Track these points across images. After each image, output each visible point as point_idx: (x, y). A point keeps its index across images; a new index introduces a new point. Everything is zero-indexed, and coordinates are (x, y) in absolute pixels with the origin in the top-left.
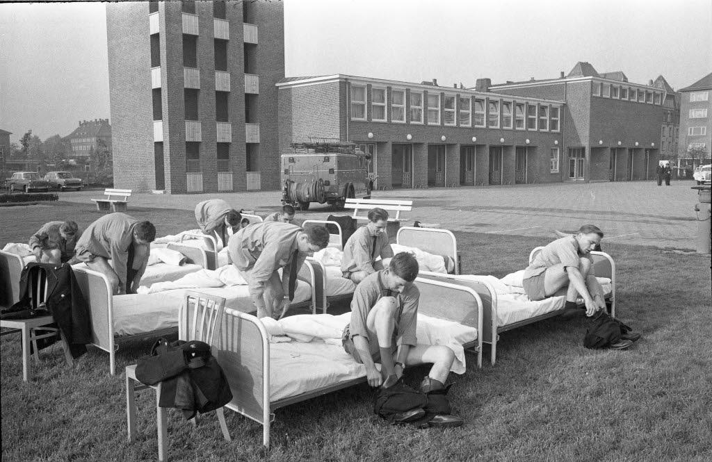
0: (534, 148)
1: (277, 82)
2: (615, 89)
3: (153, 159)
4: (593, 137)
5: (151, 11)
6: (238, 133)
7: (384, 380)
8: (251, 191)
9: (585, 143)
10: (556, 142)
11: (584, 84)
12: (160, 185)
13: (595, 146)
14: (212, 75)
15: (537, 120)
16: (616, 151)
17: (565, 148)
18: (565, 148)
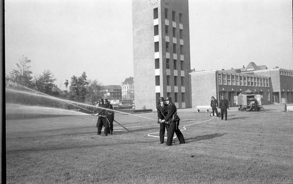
0: (263, 92)
1: (189, 73)
2: (233, 76)
3: (155, 98)
4: (281, 89)
5: (155, 35)
6: (173, 89)
7: (169, 104)
8: (183, 108)
9: (279, 90)
10: (269, 91)
11: (277, 71)
12: (162, 141)
13: (282, 91)
14: (173, 71)
15: (250, 82)
16: (288, 93)
17: (271, 92)
18: (271, 92)
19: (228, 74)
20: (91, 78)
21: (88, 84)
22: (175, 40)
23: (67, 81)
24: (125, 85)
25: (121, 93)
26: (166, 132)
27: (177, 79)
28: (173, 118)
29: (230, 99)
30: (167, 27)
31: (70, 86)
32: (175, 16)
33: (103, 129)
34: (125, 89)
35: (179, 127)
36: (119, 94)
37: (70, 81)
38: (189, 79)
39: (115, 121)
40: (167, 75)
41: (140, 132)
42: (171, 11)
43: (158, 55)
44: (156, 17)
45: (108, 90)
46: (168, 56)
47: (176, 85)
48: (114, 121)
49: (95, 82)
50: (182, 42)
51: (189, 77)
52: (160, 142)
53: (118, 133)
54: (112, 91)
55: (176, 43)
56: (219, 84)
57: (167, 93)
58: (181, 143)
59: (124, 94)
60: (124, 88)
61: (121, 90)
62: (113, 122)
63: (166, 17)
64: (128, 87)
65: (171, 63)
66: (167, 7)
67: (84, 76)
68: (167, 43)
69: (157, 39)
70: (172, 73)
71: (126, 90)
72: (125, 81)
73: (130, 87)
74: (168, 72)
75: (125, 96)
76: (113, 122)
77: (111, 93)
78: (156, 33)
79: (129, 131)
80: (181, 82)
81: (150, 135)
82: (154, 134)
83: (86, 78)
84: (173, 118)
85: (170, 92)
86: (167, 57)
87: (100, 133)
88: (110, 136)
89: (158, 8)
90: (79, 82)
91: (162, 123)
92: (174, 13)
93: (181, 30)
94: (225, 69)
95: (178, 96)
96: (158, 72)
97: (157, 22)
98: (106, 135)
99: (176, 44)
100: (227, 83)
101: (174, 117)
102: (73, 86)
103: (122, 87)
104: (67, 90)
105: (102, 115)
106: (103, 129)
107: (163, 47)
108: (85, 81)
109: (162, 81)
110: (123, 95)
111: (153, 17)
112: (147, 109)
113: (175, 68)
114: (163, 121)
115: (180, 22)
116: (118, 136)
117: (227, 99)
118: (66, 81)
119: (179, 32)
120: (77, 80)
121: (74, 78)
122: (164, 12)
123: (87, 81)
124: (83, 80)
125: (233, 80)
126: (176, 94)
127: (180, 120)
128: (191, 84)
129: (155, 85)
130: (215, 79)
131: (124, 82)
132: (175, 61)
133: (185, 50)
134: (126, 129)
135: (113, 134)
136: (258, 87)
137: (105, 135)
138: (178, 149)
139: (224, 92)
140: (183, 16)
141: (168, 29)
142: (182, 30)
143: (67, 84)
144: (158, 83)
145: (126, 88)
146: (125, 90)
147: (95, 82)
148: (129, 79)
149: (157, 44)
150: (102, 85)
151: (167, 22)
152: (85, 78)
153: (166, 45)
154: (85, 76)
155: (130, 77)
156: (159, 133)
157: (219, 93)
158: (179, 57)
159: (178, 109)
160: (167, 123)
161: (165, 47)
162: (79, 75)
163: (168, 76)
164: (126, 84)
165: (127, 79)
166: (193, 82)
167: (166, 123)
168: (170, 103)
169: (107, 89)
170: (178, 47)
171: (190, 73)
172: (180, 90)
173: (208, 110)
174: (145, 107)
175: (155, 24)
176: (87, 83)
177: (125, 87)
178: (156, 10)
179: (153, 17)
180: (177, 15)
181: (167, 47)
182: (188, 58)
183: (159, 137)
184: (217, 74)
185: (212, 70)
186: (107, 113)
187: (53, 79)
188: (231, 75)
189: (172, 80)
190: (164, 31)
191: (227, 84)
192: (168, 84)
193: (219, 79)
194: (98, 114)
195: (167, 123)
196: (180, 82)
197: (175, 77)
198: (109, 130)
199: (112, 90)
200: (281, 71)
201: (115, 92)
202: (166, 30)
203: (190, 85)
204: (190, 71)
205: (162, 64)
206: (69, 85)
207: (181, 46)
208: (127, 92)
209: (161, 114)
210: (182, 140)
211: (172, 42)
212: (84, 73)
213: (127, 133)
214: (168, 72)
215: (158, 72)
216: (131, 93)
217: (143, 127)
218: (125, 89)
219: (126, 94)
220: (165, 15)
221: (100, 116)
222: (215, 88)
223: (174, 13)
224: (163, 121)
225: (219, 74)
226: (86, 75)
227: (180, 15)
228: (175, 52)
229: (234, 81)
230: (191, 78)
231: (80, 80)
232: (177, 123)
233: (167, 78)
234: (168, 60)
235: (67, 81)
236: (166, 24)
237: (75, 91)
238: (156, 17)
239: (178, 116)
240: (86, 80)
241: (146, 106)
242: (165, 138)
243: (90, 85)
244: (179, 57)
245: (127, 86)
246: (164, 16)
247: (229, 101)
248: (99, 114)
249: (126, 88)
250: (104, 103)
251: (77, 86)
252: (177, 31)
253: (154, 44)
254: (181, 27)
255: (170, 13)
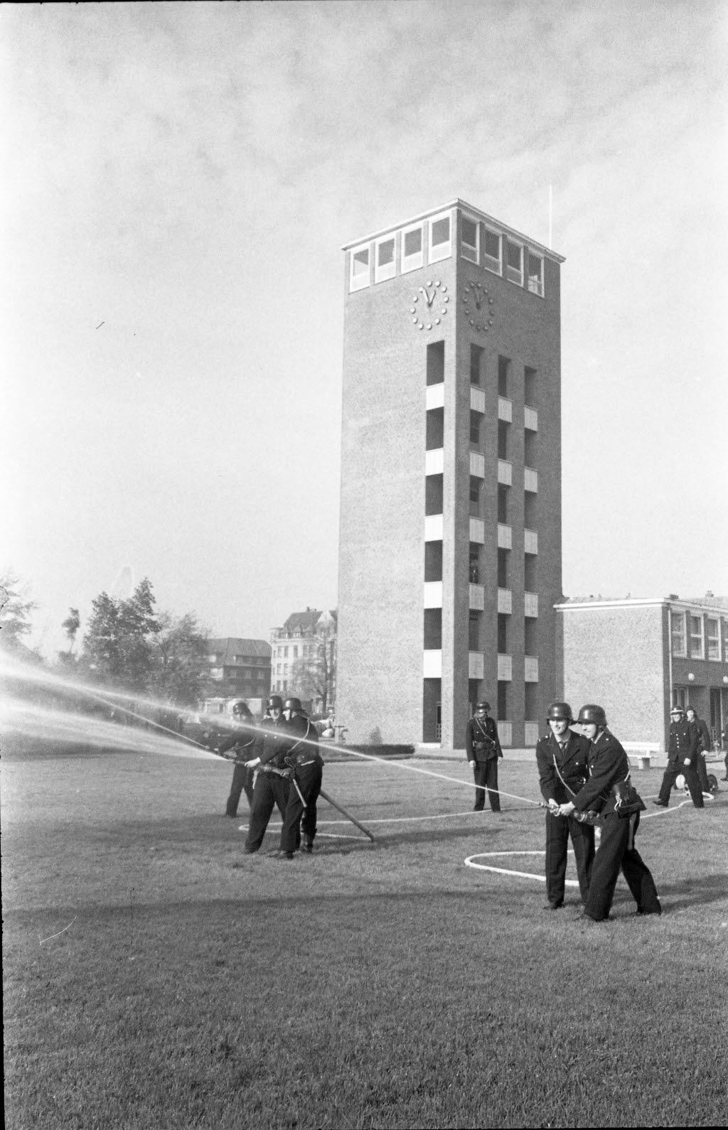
7: (595, 737)
19: (711, 615)
20: (171, 606)
21: (157, 631)
22: (505, 473)
23: (75, 612)
24: (285, 641)
25: (268, 672)
26: (571, 852)
27: (510, 625)
28: (619, 800)
29: (716, 713)
30: (476, 417)
31: (88, 634)
32: (509, 377)
33: (276, 825)
34: (286, 655)
35: (637, 838)
36: (261, 676)
37: (88, 614)
38: (553, 629)
39: (325, 797)
40: (472, 607)
41: (426, 848)
42: (495, 358)
43: (439, 528)
44: (435, 375)
45: (219, 655)
46: (477, 531)
47: (502, 649)
48: (319, 796)
49: (188, 624)
50: (531, 481)
51: (554, 620)
52: (546, 903)
53: (332, 848)
54: (234, 661)
55: (508, 482)
56: (676, 655)
57: (467, 682)
58: (642, 910)
59: (282, 678)
60: (279, 650)
61: (267, 659)
62: (318, 800)
63: (475, 379)
64: (296, 649)
65: (488, 564)
66: (480, 341)
67: (145, 597)
68: (476, 482)
69: (440, 461)
70: (491, 603)
71: (291, 660)
72: (285, 625)
73: (304, 648)
74: (476, 597)
75: (285, 683)
76: (316, 797)
77: (227, 669)
78: (435, 440)
79: (378, 843)
80: (526, 638)
81: (472, 861)
82: (485, 858)
83: (152, 605)
84: (619, 800)
85: (481, 676)
86: (473, 539)
87: (256, 842)
88: (301, 862)
89: (446, 344)
90: (121, 622)
91: (561, 816)
92: (504, 364)
93: (529, 433)
94: (681, 598)
95: (509, 693)
96: (439, 595)
97: (440, 396)
98: (290, 856)
99: (508, 487)
100: (707, 651)
101: (621, 797)
102: (98, 634)
103: (274, 647)
104: (73, 652)
105: (272, 765)
106: (276, 825)
107: (458, 498)
108: (147, 616)
109: (452, 631)
110: (274, 679)
111: (424, 376)
112: (387, 741)
113: (502, 583)
114: (566, 808)
115: (528, 401)
116: (341, 862)
117: (705, 717)
118: (68, 615)
119: (522, 440)
120: (114, 612)
121: (104, 605)
122: (467, 358)
123: (154, 618)
124: (139, 614)
125: (711, 638)
126: (503, 685)
127: (644, 808)
128: (562, 651)
129: (422, 644)
130: (660, 634)
131: (282, 626)
132: (503, 554)
133: (542, 511)
134: (360, 826)
135: (314, 850)
136: (706, 662)
137: (282, 853)
138: (628, 934)
139: (694, 689)
140: (538, 376)
141: (482, 426)
142: (534, 432)
143: (73, 625)
144: (433, 640)
145: (291, 651)
146: (282, 661)
147: (188, 624)
148: (302, 614)
149: (435, 482)
150: (211, 637)
151: (478, 400)
152: (147, 604)
153: (472, 489)
154: (147, 595)
155: (308, 609)
156: (544, 853)
157: (675, 691)
158: (518, 538)
159: (507, 748)
160: (584, 817)
161: (466, 494)
162: (123, 594)
163: (475, 615)
164: (290, 636)
165: (294, 615)
166: (570, 643)
167: (576, 820)
168: (600, 735)
169: (213, 653)
170: (515, 501)
171: (562, 606)
172: (518, 671)
173: (646, 761)
174: (376, 735)
175: (432, 405)
176: (155, 627)
177: (286, 648)
178: (436, 350)
179: (425, 375)
180: (516, 374)
181: (474, 496)
182: (553, 543)
183: (543, 879)
184: (669, 612)
185: (628, 597)
186: (295, 761)
187: (24, 603)
188: (702, 618)
189: (488, 630)
190: (466, 432)
191: (707, 654)
192: (474, 646)
193: (674, 632)
194: (258, 760)
195: (584, 817)
196: (522, 641)
197: (503, 618)
198: (301, 834)
199: (235, 658)
200: (671, 613)
201: (245, 665)
202: (473, 425)
203: (558, 653)
204: (562, 599)
205: (452, 564)
206: (84, 630)
207: (529, 495)
208: (294, 667)
209: (554, 776)
210: (647, 899)
211: (495, 477)
212: (145, 585)
213: (372, 848)
214: (476, 597)
215: (439, 595)
216: (308, 674)
217: (424, 823)
218: (286, 655)
219: (289, 677)
220: (472, 374)
221: (266, 768)
222: (660, 669)
223: (504, 364)
224: (566, 808)
225: (673, 615)
226: (152, 591)
227: (529, 372)
228: (503, 519)
229: (715, 643)
230: (562, 625)
231: (128, 611)
232: (632, 822)
233: (471, 619)
234: (475, 549)
235: (75, 612)
236: (474, 407)
237: (107, 655)
238: (435, 375)
239: (634, 789)
240: (150, 611)
241: (382, 730)
242: (568, 883)
243: (164, 634)
244: (518, 538)
245: (295, 644)
246: (468, 377)
247: (713, 724)
248: (264, 762)
249: (291, 651)
250: (287, 713)
251: (113, 637)
252: (515, 437)
253: (423, 482)
254: (531, 420)
255: (490, 369)
